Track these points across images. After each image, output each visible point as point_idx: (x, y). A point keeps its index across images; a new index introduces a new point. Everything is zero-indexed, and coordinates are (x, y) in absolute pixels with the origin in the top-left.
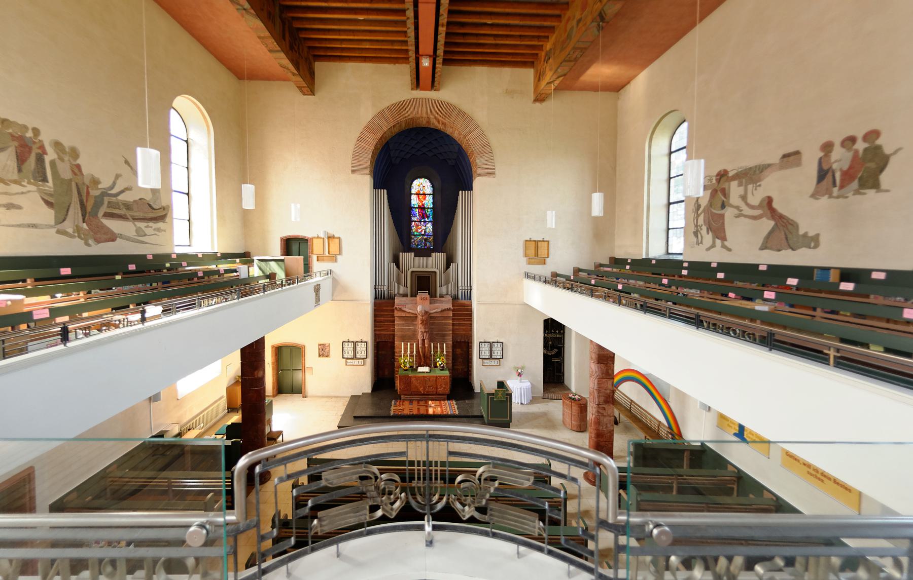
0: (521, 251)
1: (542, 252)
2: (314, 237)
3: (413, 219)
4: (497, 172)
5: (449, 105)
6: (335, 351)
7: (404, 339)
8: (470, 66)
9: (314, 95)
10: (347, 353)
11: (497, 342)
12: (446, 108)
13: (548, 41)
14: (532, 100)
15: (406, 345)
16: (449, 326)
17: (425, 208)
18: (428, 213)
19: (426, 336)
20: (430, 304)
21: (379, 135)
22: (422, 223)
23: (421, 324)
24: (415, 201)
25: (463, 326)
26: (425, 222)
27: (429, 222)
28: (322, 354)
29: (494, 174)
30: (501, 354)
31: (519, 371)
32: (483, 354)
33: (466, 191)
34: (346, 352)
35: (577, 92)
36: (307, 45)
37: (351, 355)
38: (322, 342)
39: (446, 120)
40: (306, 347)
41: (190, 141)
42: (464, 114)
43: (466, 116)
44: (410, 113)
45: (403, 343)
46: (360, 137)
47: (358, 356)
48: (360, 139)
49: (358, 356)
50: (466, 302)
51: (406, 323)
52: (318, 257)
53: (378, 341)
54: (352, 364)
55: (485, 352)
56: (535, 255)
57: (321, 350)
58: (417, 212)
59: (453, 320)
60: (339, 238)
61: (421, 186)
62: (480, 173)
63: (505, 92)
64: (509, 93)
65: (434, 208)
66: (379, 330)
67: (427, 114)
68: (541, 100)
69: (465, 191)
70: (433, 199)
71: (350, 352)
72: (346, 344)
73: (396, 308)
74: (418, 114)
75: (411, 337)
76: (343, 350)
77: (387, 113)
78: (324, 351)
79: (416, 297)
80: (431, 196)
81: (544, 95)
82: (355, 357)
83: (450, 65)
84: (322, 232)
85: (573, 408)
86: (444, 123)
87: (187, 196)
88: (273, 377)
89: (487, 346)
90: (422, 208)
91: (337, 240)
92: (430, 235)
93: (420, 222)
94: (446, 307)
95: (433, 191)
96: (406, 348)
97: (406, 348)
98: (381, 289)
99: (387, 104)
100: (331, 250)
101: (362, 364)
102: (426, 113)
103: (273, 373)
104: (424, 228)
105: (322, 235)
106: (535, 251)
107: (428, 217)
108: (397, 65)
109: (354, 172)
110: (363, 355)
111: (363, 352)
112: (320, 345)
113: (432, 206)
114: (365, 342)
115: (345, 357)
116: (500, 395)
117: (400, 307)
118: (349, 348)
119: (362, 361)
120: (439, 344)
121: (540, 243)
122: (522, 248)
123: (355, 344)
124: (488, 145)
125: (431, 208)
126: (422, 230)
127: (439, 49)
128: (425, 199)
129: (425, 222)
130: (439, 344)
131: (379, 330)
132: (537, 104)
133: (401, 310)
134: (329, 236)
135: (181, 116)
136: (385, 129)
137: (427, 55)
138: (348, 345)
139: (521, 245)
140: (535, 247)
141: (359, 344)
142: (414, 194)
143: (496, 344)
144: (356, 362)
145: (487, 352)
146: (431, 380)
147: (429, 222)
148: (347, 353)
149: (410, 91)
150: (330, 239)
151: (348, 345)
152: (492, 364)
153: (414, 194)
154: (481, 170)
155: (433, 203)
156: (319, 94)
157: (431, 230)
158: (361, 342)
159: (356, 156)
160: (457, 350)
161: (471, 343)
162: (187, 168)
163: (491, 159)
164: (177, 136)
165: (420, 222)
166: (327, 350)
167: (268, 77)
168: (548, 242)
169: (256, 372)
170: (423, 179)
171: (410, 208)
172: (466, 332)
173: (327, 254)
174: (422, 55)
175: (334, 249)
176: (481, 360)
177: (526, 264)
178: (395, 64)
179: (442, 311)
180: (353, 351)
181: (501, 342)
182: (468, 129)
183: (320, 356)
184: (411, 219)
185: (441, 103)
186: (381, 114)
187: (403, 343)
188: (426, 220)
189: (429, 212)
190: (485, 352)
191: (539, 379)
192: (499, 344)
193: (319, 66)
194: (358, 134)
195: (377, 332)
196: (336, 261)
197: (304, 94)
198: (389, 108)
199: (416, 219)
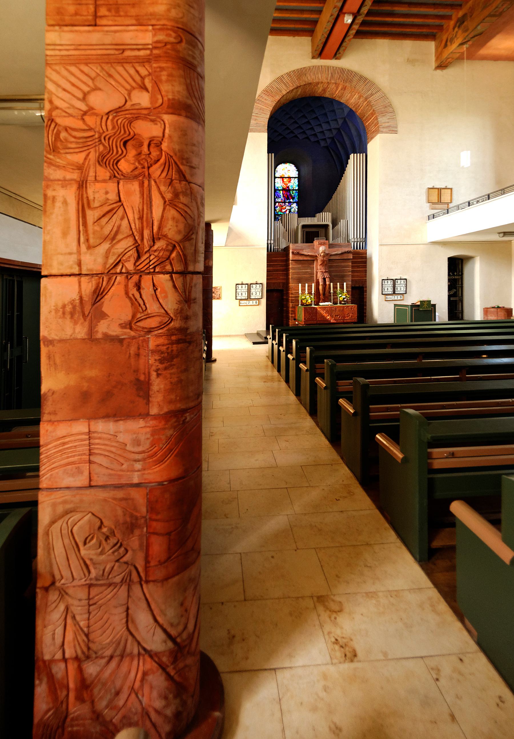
0: (424, 198)
1: (445, 198)
4: (399, 129)
5: (350, 72)
7: (300, 280)
8: (371, 39)
13: (461, 9)
14: (434, 67)
17: (289, 190)
18: (293, 195)
19: (326, 275)
21: (278, 98)
22: (287, 204)
23: (321, 265)
25: (357, 272)
26: (290, 202)
29: (397, 131)
30: (405, 290)
32: (386, 290)
33: (355, 154)
34: (240, 294)
35: (477, 61)
42: (366, 79)
44: (310, 78)
45: (300, 285)
47: (252, 297)
49: (252, 297)
50: (361, 251)
51: (303, 267)
54: (246, 304)
55: (388, 289)
56: (438, 201)
58: (281, 194)
59: (353, 263)
62: (381, 129)
63: (406, 61)
64: (411, 61)
65: (299, 191)
67: (327, 79)
68: (444, 66)
70: (298, 182)
71: (244, 294)
72: (240, 286)
75: (309, 279)
77: (287, 79)
79: (313, 243)
80: (296, 179)
81: (450, 59)
82: (249, 298)
85: (499, 313)
89: (390, 283)
90: (286, 190)
93: (285, 202)
95: (299, 174)
98: (271, 243)
101: (257, 304)
102: (327, 79)
104: (289, 208)
106: (438, 197)
107: (293, 198)
108: (296, 37)
110: (259, 296)
111: (258, 293)
113: (297, 188)
114: (260, 284)
115: (238, 298)
116: (426, 305)
119: (257, 301)
120: (338, 284)
121: (442, 190)
122: (425, 194)
124: (391, 106)
126: (287, 210)
128: (289, 182)
129: (290, 202)
130: (338, 284)
132: (439, 72)
136: (284, 92)
138: (242, 287)
139: (424, 191)
140: (438, 194)
142: (279, 178)
143: (399, 281)
144: (251, 302)
147: (294, 203)
148: (240, 294)
149: (310, 59)
151: (242, 287)
152: (395, 299)
153: (279, 178)
155: (298, 186)
157: (297, 210)
161: (366, 287)
163: (394, 118)
165: (285, 202)
166: (218, 293)
168: (451, 189)
172: (360, 278)
177: (430, 209)
178: (294, 36)
179: (342, 254)
180: (247, 293)
181: (404, 279)
182: (370, 92)
185: (342, 70)
186: (280, 79)
187: (300, 285)
188: (291, 200)
189: (294, 194)
191: (444, 310)
198: (289, 74)
199: (280, 200)
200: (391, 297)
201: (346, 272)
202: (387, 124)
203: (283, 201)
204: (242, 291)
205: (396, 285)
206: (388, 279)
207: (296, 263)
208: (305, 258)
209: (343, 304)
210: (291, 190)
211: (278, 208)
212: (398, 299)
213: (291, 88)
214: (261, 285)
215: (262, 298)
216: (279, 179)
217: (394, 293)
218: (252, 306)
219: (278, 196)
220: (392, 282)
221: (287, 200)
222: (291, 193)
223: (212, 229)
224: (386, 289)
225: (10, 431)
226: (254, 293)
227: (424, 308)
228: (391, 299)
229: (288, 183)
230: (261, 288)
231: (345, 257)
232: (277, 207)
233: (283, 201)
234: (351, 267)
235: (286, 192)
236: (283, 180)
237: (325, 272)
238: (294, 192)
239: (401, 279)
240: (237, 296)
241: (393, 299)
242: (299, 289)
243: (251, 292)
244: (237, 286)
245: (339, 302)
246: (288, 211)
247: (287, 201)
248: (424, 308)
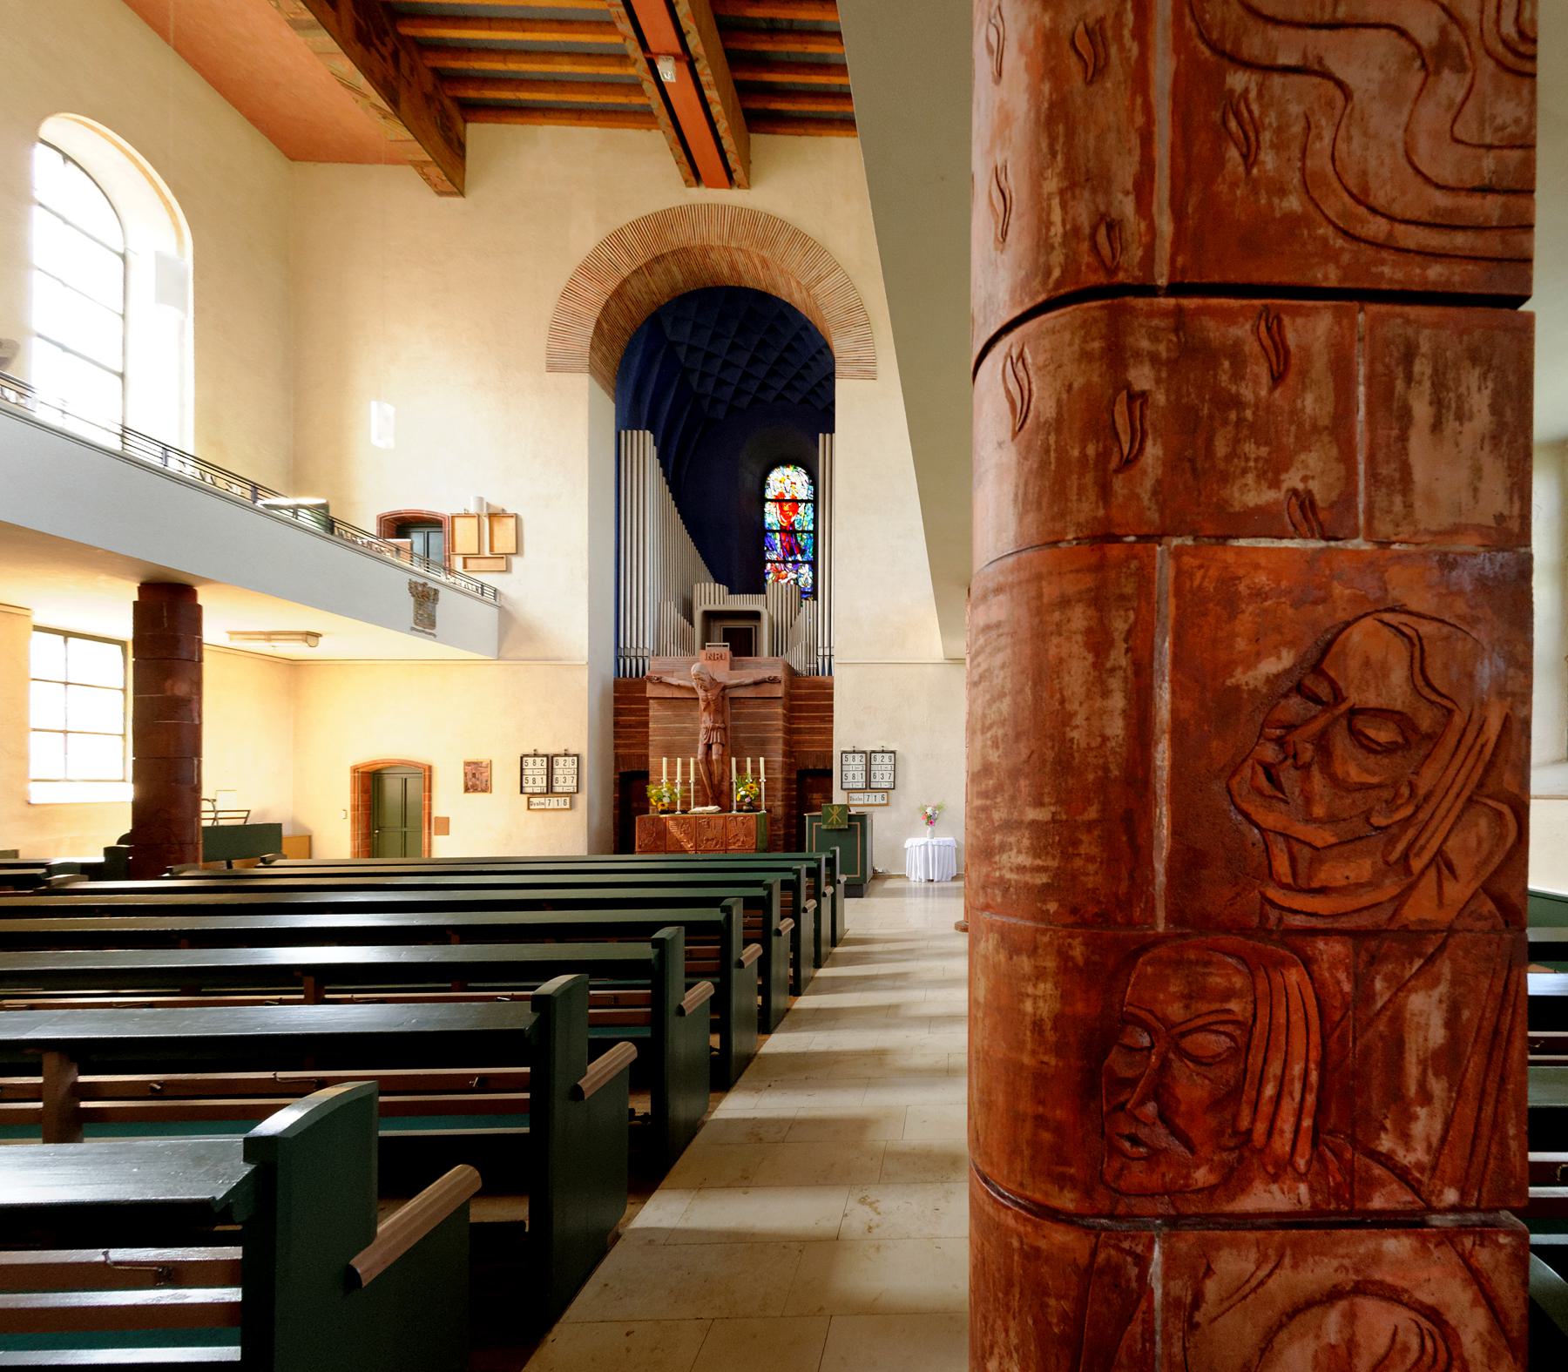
2: (459, 516)
3: (768, 556)
5: (771, 219)
6: (504, 778)
7: (670, 751)
8: (821, 135)
9: (461, 193)
10: (530, 783)
11: (883, 752)
12: (766, 227)
15: (672, 766)
16: (777, 720)
18: (803, 544)
19: (716, 737)
20: (732, 668)
22: (790, 566)
24: (772, 516)
26: (795, 563)
27: (804, 563)
28: (473, 786)
29: (874, 372)
31: (929, 811)
32: (850, 779)
34: (530, 778)
36: (429, 64)
37: (541, 783)
38: (472, 758)
39: (766, 254)
40: (434, 770)
41: (131, 257)
42: (806, 238)
43: (810, 243)
44: (681, 237)
45: (665, 759)
46: (568, 289)
48: (567, 293)
49: (558, 789)
51: (677, 716)
52: (465, 559)
53: (622, 770)
54: (543, 807)
55: (854, 776)
57: (470, 776)
58: (778, 542)
60: (516, 516)
61: (788, 482)
66: (625, 746)
69: (825, 434)
71: (538, 779)
72: (530, 760)
73: (649, 679)
74: (702, 238)
76: (522, 775)
78: (476, 779)
82: (550, 790)
83: (774, 133)
84: (472, 498)
86: (764, 262)
87: (119, 380)
88: (353, 839)
90: (789, 531)
91: (512, 521)
92: (808, 593)
93: (785, 562)
94: (767, 676)
96: (672, 773)
97: (672, 773)
98: (636, 657)
99: (629, 216)
100: (496, 544)
102: (721, 237)
103: (353, 830)
104: (795, 576)
105: (473, 510)
107: (803, 552)
109: (552, 368)
111: (569, 778)
112: (467, 764)
114: (574, 755)
116: (835, 817)
117: (658, 676)
118: (536, 770)
119: (568, 799)
123: (550, 760)
125: (809, 532)
127: (689, 32)
128: (795, 511)
129: (795, 563)
131: (625, 746)
133: (660, 682)
134: (492, 511)
135: (94, 181)
137: (668, 54)
141: (561, 760)
142: (772, 501)
143: (879, 756)
144: (553, 802)
145: (858, 775)
146: (712, 823)
147: (804, 563)
150: (495, 520)
152: (870, 802)
153: (772, 501)
154: (845, 364)
156: (475, 193)
158: (566, 755)
159: (557, 331)
160: (815, 796)
162: (123, 317)
164: (89, 232)
165: (785, 562)
167: (353, 153)
169: (168, 683)
170: (792, 468)
171: (762, 532)
173: (487, 554)
174: (658, 54)
175: (505, 541)
176: (845, 793)
178: (649, 129)
179: (756, 684)
180: (545, 777)
182: (814, 273)
183: (467, 790)
184: (765, 556)
185: (752, 219)
186: (616, 238)
187: (665, 759)
188: (799, 557)
190: (854, 776)
192: (887, 756)
193: (478, 134)
194: (563, 283)
195: (621, 751)
196: (508, 570)
197: (441, 193)
198: (634, 226)
199: (774, 557)
200: (861, 796)
201: (769, 731)
202: (853, 356)
203: (781, 559)
204: (536, 772)
205: (873, 767)
206: (854, 752)
207: (660, 705)
208: (678, 694)
209: (747, 811)
210: (799, 532)
211: (771, 575)
212: (877, 802)
213: (641, 262)
214: (575, 758)
215: (578, 792)
216: (773, 505)
217: (868, 787)
218: (560, 813)
219: (771, 546)
220: (864, 760)
221: (791, 555)
222: (799, 539)
223: (200, 601)
224: (850, 775)
225: (585, 1074)
226: (561, 779)
227: (832, 823)
228: (861, 802)
229: (791, 514)
230: (575, 766)
231: (766, 691)
232: (769, 573)
233: (781, 559)
234: (781, 717)
235: (787, 536)
236: (781, 508)
237: (713, 729)
238: (805, 536)
239: (883, 752)
240: (524, 785)
241: (866, 802)
242: (662, 773)
243: (555, 777)
244: (525, 759)
245: (735, 808)
246: (792, 582)
247: (790, 559)
248: (832, 823)
